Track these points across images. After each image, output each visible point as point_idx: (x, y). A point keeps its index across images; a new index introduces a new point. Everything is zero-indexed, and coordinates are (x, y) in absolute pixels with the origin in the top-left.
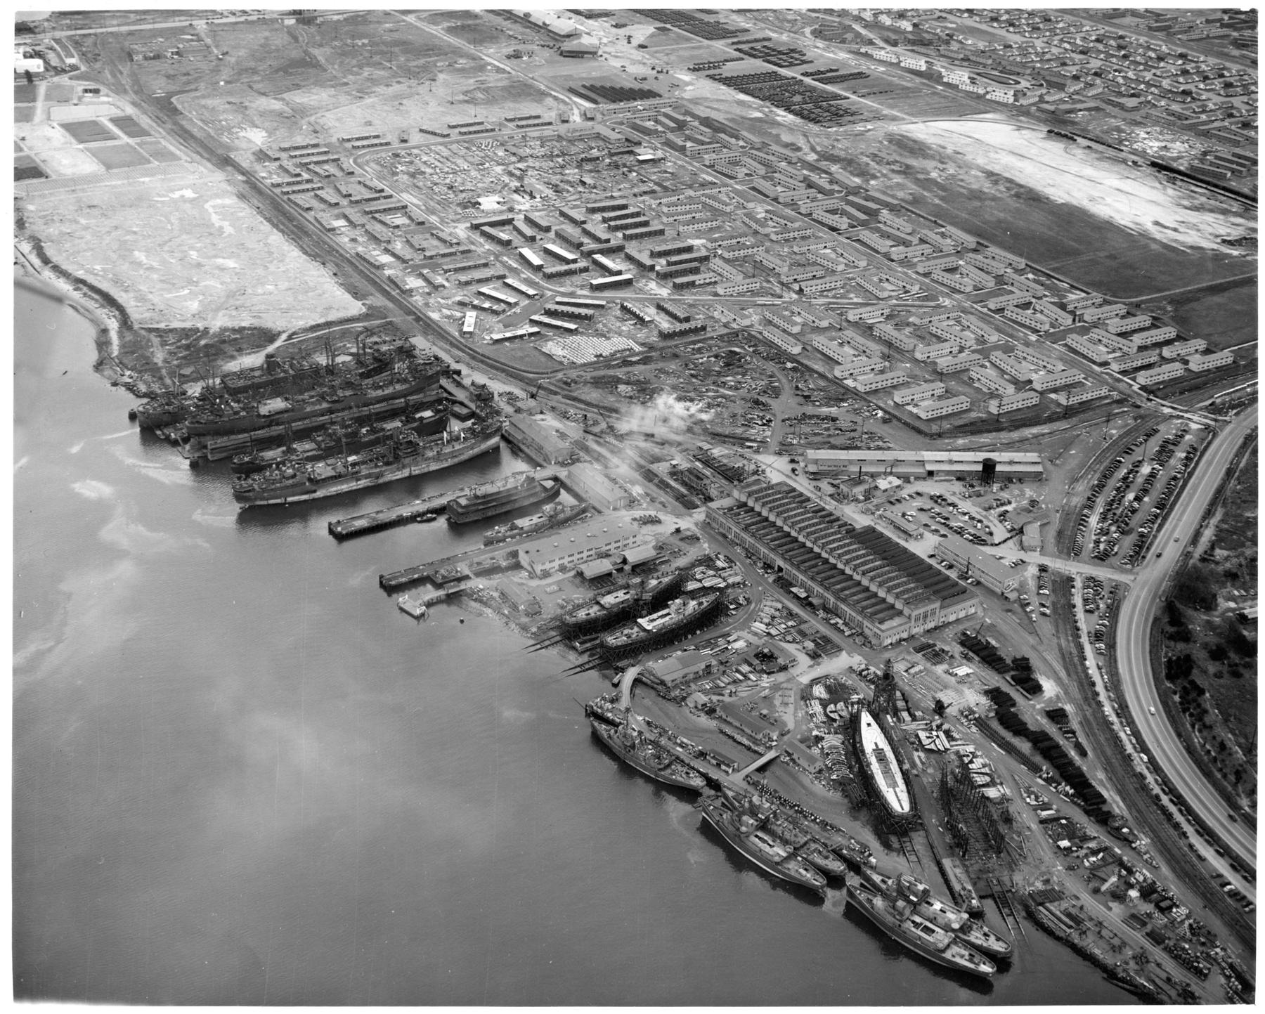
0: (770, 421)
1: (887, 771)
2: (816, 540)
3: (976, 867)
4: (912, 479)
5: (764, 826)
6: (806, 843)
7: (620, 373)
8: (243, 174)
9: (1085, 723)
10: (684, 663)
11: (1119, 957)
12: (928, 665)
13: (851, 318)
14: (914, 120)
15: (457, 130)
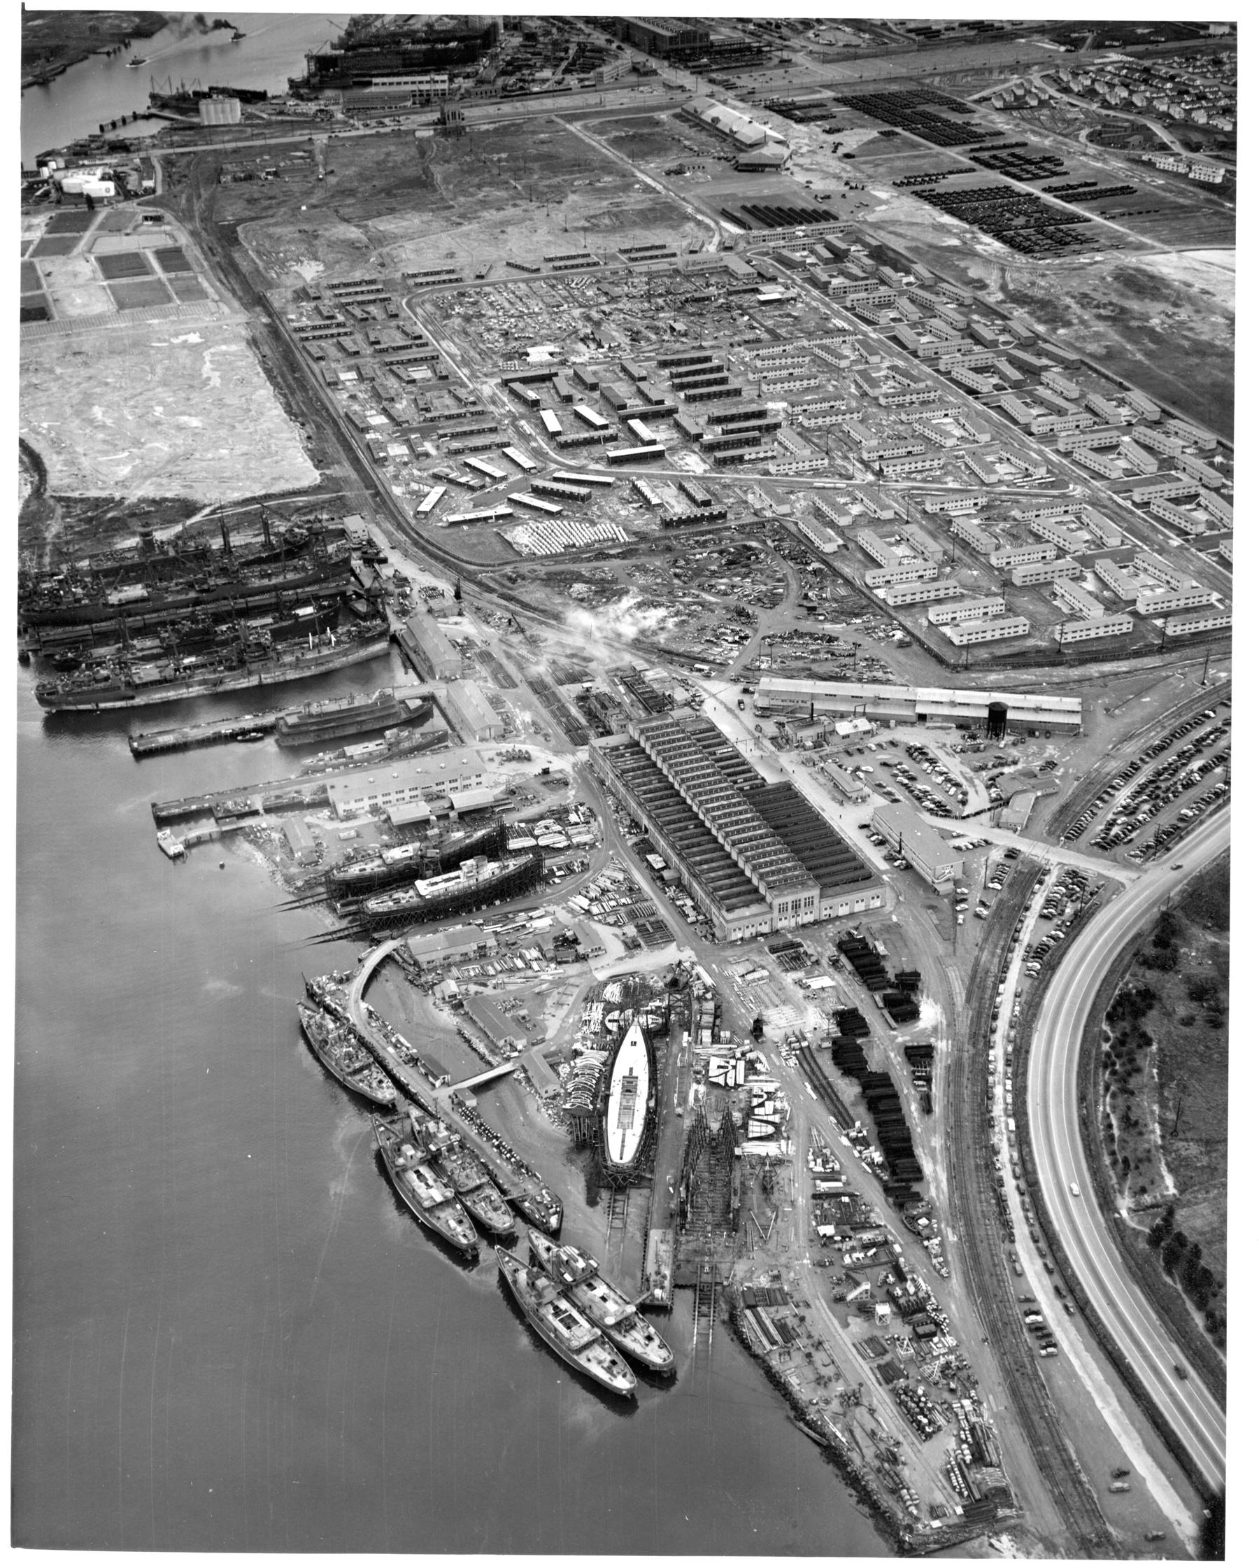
0: (746, 637)
1: (627, 1109)
2: (695, 795)
3: (692, 1246)
4: (892, 723)
5: (433, 1161)
6: (478, 1187)
7: (584, 569)
8: (270, 315)
9: (955, 1070)
10: (453, 941)
11: (821, 1392)
12: (778, 971)
13: (929, 508)
14: (1166, 248)
15: (551, 265)
